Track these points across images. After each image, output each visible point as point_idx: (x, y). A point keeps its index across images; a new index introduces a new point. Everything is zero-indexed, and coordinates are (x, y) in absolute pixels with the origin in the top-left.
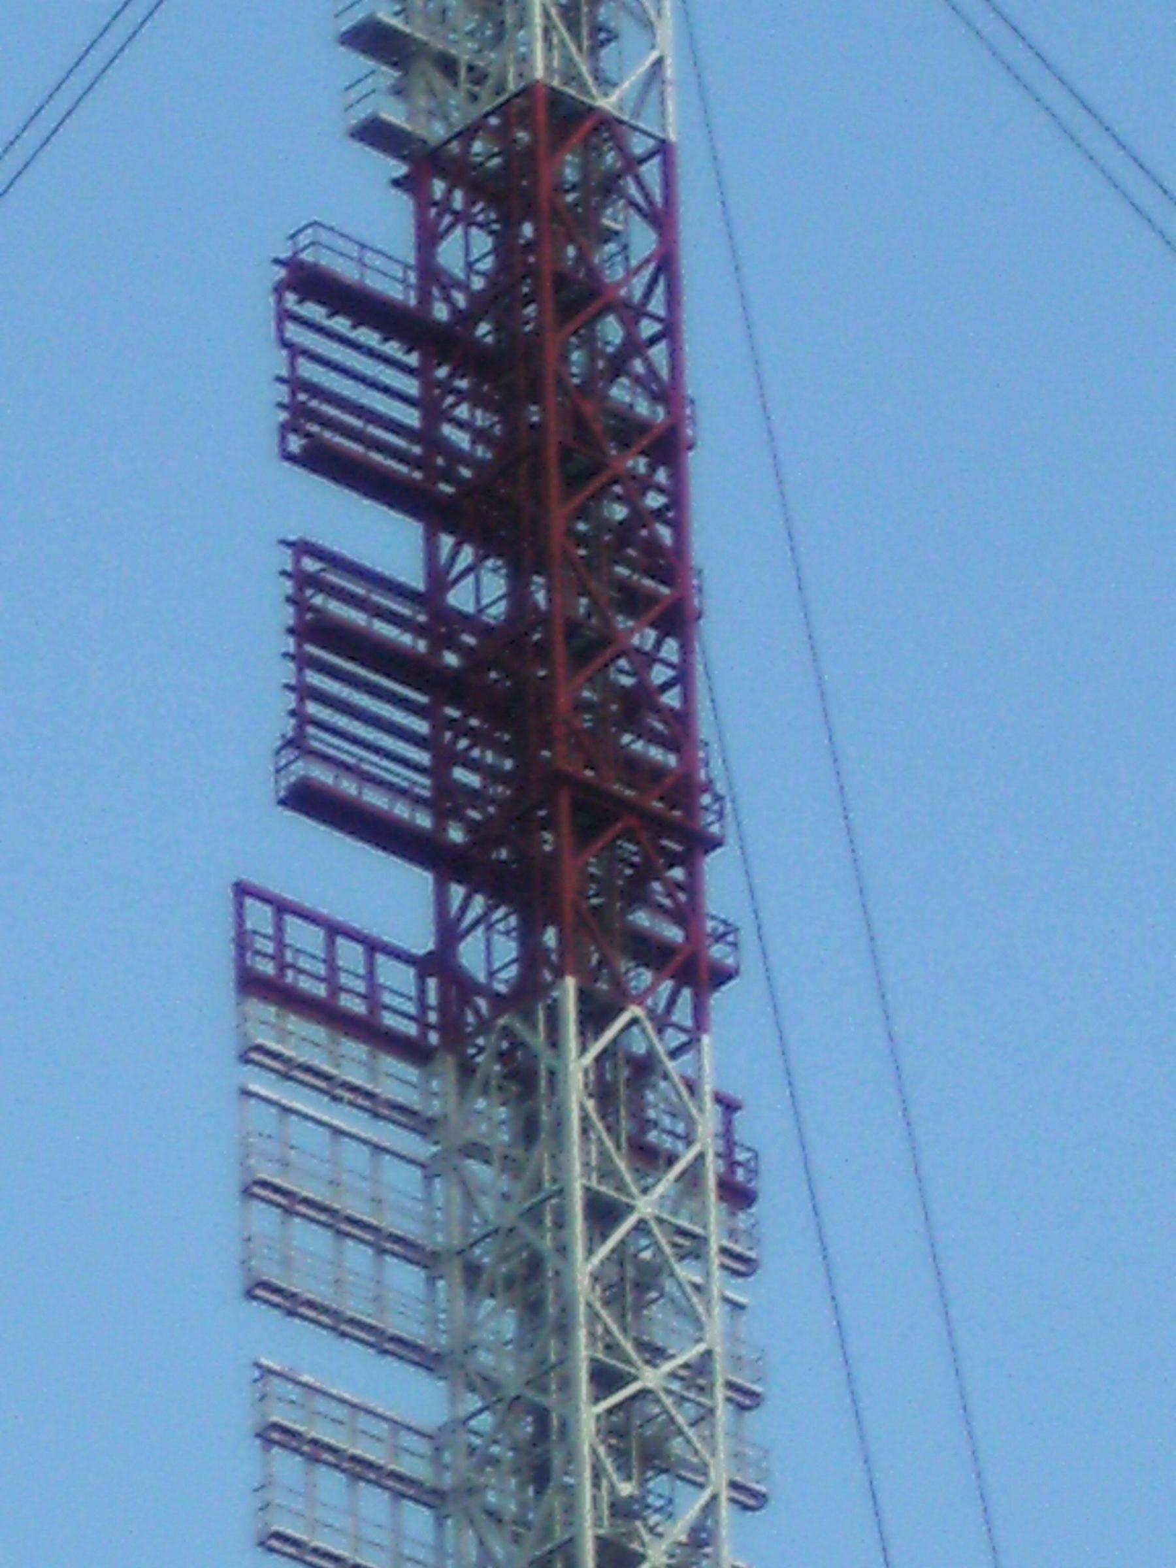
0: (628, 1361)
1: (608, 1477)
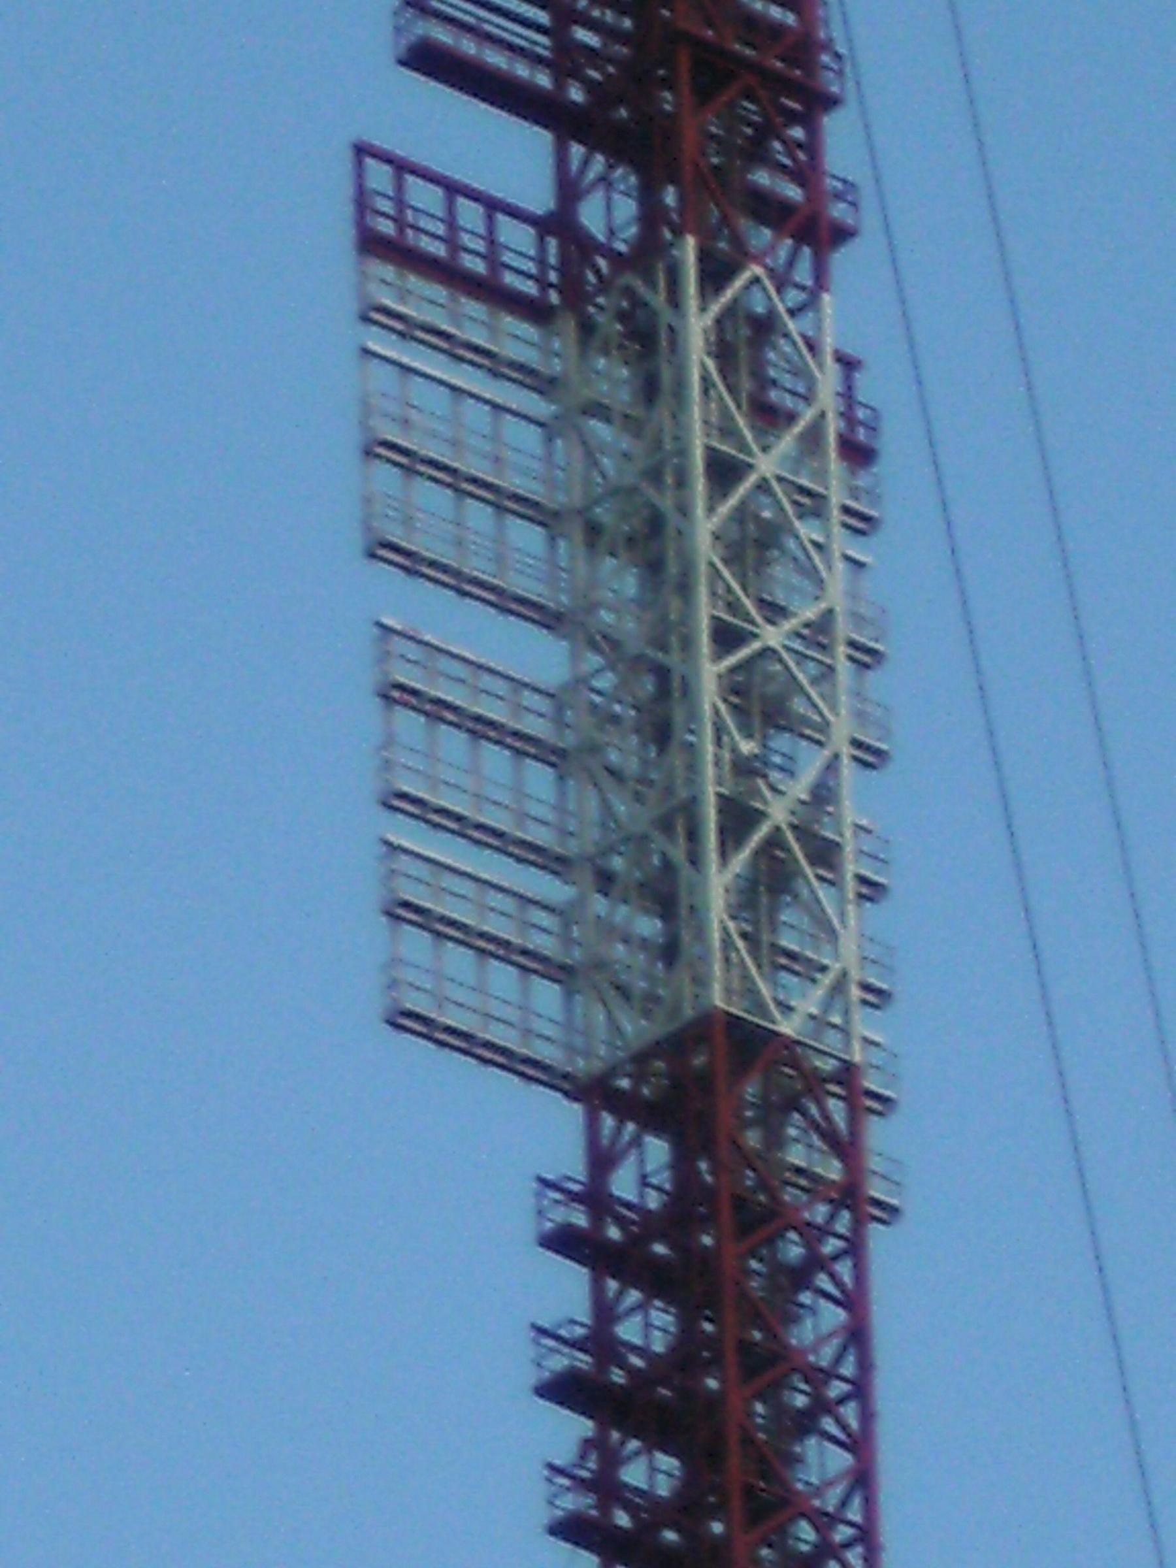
1: (729, 734)
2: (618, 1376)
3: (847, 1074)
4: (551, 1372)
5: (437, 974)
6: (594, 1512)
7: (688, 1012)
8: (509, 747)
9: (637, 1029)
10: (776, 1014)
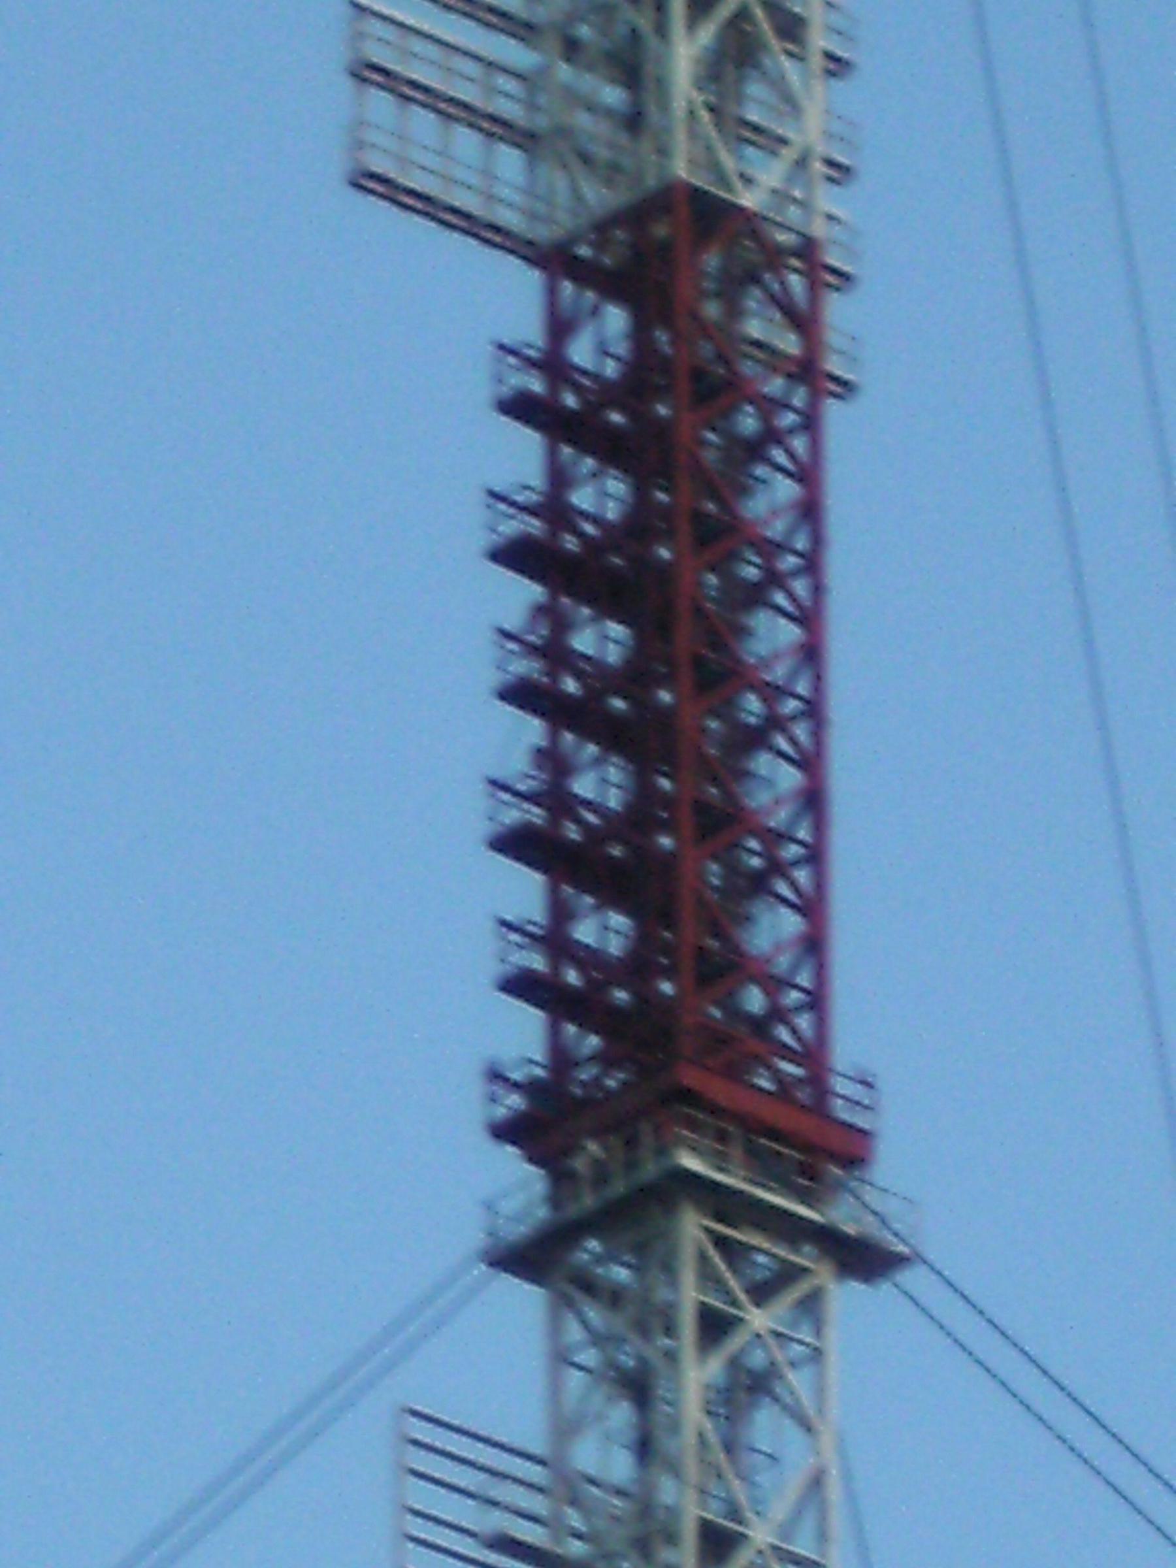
0: (734, 1303)
2: (570, 543)
3: (808, 249)
4: (510, 1108)
5: (402, 137)
6: (545, 680)
7: (651, 182)
8: (481, 130)
9: (599, 197)
10: (738, 185)
